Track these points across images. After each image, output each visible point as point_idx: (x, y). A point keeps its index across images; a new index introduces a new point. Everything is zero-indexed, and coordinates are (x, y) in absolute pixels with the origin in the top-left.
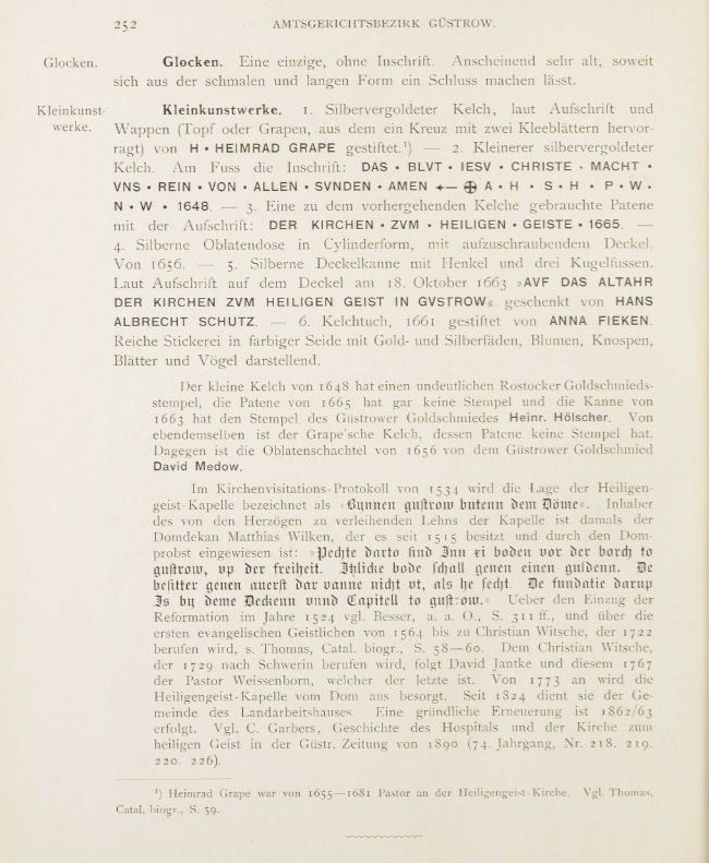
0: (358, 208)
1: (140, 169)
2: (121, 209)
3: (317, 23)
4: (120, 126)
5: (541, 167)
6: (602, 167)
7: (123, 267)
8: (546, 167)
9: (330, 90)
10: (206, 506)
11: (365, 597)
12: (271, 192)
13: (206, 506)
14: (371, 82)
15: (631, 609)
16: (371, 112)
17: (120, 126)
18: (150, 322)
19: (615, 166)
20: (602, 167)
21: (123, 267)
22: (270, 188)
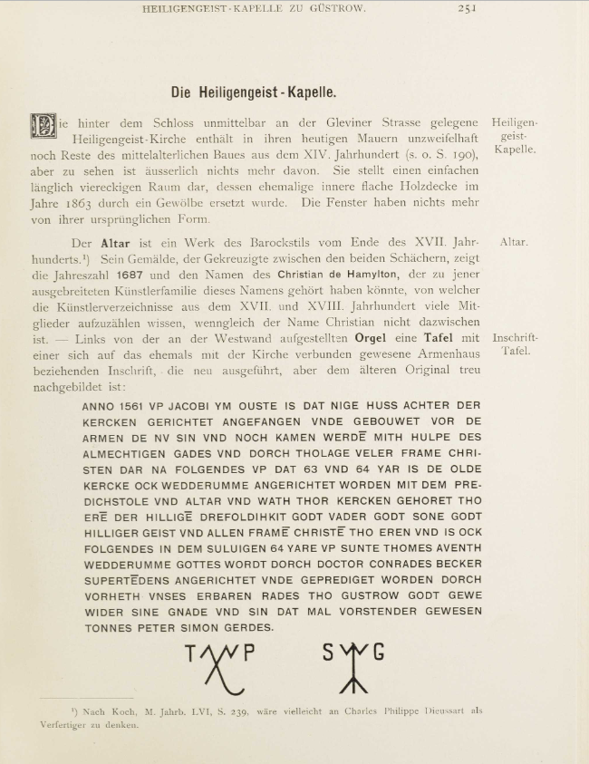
0: (322, 470)
1: (460, 291)
2: (163, 456)
3: (180, 8)
4: (189, 240)
5: (319, 533)
6: (317, 612)
7: (46, 726)
8: (323, 533)
9: (135, 228)
10: (509, 150)
11: (469, 301)
12: (166, 522)
13: (509, 150)
14: (189, 220)
15: (460, 426)
16: (119, 341)
17: (189, 240)
18: (310, 549)
19: (414, 405)
20: (317, 612)
21: (46, 726)
22: (103, 534)
